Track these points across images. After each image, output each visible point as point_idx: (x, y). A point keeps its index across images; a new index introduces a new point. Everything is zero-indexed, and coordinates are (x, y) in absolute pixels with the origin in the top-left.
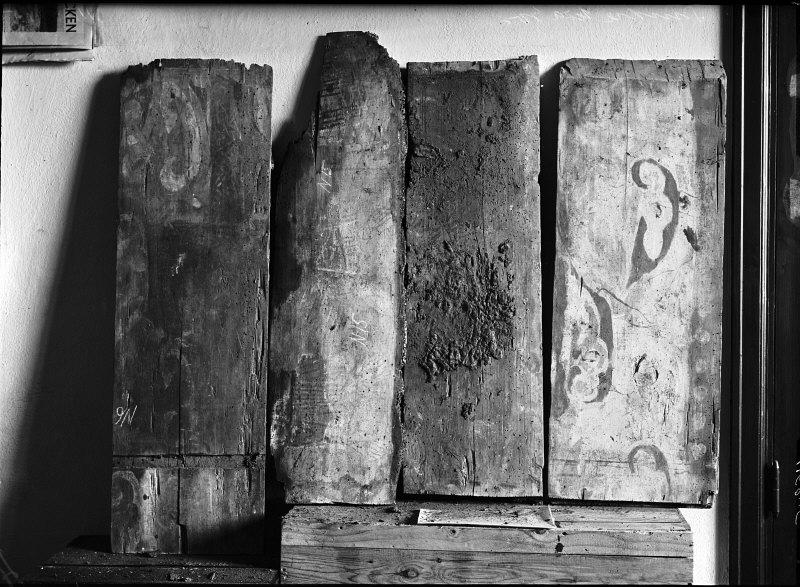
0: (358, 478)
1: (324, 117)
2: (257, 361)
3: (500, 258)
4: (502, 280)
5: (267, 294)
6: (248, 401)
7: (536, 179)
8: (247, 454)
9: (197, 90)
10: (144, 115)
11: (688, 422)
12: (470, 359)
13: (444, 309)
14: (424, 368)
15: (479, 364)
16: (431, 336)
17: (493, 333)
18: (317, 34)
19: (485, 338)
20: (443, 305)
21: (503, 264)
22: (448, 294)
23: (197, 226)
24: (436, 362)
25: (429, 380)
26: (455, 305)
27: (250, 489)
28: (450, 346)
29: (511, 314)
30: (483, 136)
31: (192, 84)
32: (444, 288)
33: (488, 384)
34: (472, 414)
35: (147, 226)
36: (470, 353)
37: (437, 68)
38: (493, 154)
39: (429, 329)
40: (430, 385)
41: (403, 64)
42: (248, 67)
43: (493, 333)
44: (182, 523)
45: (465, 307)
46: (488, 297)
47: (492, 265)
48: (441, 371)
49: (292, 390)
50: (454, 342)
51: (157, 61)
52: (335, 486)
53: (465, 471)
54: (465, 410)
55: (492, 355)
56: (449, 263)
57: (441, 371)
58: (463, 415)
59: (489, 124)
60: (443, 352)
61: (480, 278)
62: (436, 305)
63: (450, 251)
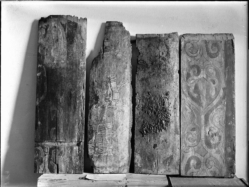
0: (117, 164)
1: (105, 48)
2: (81, 112)
3: (166, 97)
4: (167, 105)
5: (85, 90)
6: (79, 125)
7: (178, 72)
8: (78, 141)
9: (63, 25)
10: (46, 33)
11: (226, 149)
12: (156, 130)
13: (148, 113)
14: (141, 132)
15: (159, 131)
16: (144, 122)
17: (164, 121)
18: (102, 22)
19: (161, 123)
20: (148, 112)
21: (167, 99)
22: (150, 109)
23: (64, 68)
24: (145, 130)
25: (143, 136)
26: (151, 112)
27: (79, 153)
28: (150, 125)
29: (169, 115)
30: (161, 58)
31: (61, 23)
32: (148, 107)
33: (162, 139)
34: (157, 148)
35: (46, 67)
36: (156, 128)
37: (146, 36)
38: (164, 63)
39: (143, 120)
40: (144, 138)
41: (133, 34)
42: (79, 18)
43: (164, 121)
44: (57, 163)
45: (155, 113)
46: (162, 110)
47: (164, 100)
48: (147, 133)
49: (96, 136)
50: (151, 124)
51: (50, 16)
52: (110, 167)
53: (154, 166)
54: (155, 146)
55: (163, 128)
56: (150, 98)
57: (147, 133)
58: (154, 148)
59: (163, 54)
60: (148, 127)
61: (160, 103)
62: (145, 112)
63: (150, 95)
